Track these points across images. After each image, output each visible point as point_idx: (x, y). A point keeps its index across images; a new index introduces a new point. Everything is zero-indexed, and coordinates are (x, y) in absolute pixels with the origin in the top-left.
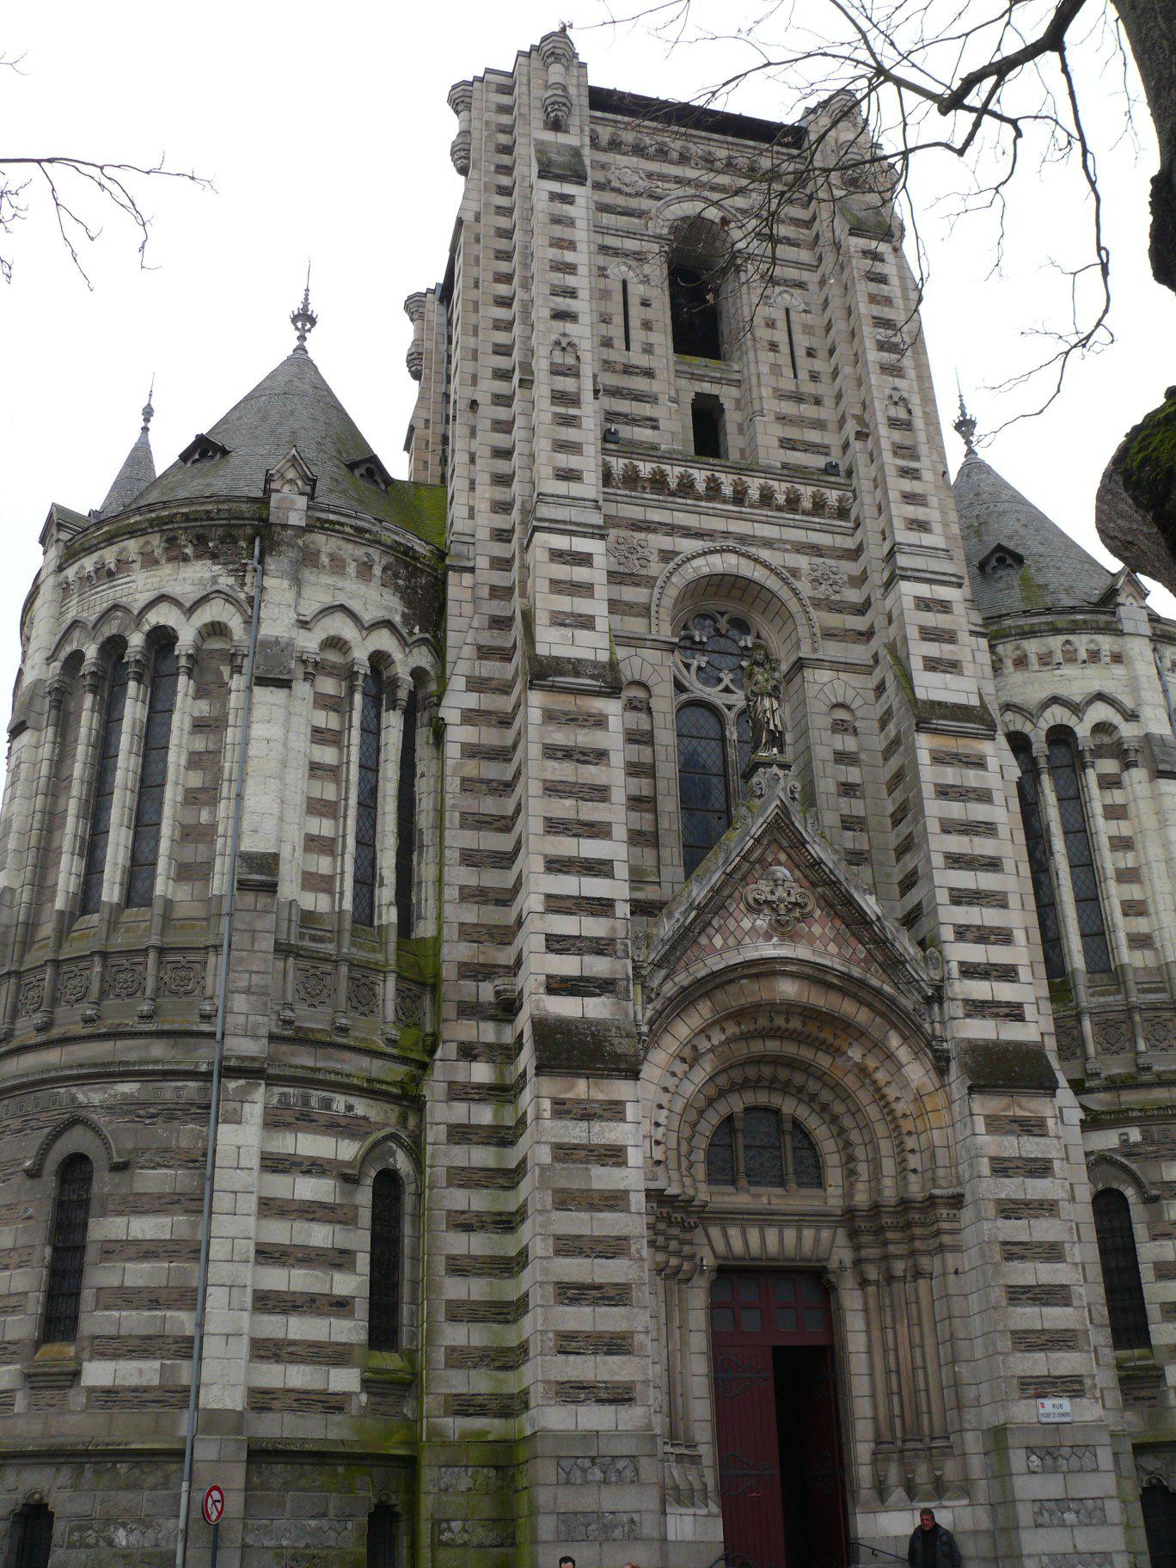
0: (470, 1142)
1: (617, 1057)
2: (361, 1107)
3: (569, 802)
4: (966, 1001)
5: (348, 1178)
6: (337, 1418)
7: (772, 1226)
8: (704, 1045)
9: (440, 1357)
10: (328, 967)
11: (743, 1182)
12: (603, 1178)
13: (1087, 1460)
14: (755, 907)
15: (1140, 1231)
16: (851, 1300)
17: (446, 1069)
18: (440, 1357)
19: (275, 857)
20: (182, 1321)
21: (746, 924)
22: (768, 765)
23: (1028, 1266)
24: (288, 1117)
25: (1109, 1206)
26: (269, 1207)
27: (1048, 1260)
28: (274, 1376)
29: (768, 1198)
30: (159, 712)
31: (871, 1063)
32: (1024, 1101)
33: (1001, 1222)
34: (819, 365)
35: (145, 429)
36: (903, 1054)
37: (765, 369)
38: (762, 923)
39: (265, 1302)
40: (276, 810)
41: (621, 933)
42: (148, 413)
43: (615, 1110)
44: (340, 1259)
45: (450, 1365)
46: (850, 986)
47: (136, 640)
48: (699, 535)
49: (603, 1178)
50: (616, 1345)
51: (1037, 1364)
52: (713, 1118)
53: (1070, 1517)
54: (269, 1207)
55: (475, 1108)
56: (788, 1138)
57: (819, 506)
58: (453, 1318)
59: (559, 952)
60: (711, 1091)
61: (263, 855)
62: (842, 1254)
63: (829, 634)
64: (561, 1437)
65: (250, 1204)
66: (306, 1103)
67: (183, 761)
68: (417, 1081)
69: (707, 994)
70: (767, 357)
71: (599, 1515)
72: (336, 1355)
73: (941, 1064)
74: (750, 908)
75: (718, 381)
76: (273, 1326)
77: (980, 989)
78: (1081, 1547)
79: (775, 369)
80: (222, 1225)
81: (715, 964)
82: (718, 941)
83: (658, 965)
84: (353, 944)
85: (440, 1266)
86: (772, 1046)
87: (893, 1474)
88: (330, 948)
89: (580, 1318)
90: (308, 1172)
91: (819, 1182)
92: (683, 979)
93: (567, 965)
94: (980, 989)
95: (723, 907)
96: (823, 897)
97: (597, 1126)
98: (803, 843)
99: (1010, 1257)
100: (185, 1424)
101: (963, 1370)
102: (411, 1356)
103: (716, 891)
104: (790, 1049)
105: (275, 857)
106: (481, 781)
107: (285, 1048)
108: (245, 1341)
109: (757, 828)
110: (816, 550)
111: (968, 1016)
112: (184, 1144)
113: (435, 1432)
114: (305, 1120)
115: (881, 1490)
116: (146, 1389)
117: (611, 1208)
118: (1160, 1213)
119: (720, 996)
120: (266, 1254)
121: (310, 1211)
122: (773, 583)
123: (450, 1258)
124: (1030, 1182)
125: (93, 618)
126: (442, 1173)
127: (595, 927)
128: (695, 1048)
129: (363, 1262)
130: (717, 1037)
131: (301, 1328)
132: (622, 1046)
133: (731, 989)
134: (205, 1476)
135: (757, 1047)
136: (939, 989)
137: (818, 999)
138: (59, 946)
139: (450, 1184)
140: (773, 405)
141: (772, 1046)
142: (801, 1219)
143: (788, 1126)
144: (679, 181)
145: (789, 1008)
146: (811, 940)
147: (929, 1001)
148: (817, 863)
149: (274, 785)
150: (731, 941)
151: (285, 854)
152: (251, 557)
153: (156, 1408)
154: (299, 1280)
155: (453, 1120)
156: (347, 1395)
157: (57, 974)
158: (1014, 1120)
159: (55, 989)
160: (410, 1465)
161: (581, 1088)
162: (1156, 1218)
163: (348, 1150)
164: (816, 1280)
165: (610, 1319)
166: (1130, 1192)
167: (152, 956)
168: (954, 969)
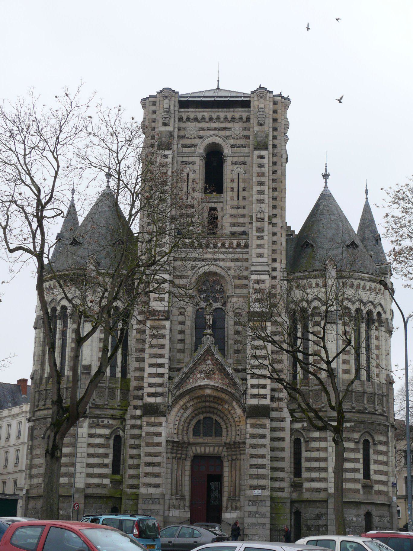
0: (135, 429)
1: (161, 412)
2: (111, 422)
3: (155, 349)
4: (251, 394)
5: (108, 438)
6: (104, 489)
7: (206, 446)
8: (188, 405)
9: (127, 476)
10: (104, 390)
11: (201, 436)
12: (156, 439)
13: (264, 504)
14: (201, 372)
15: (303, 449)
16: (226, 464)
17: (131, 411)
18: (127, 476)
19: (90, 366)
20: (72, 469)
21: (199, 376)
22: (206, 335)
23: (256, 459)
24: (94, 425)
25: (297, 444)
26: (90, 445)
27: (261, 458)
28: (91, 481)
29: (208, 440)
30: (65, 325)
31: (230, 408)
32: (261, 420)
33: (251, 449)
34: (246, 194)
35: (367, 198)
36: (236, 407)
37: (228, 199)
38: (203, 375)
39: (89, 465)
40: (90, 354)
41: (166, 382)
42: (367, 192)
43: (160, 424)
44: (106, 456)
45: (129, 478)
46: (223, 391)
47: (58, 308)
48: (203, 260)
49: (156, 439)
50: (157, 475)
51: (255, 482)
52: (195, 420)
53: (257, 516)
54: (90, 445)
55: (136, 421)
56: (214, 425)
57: (239, 245)
58: (130, 468)
59: (151, 387)
60: (193, 414)
61: (87, 365)
62: (225, 453)
63: (237, 287)
64: (144, 494)
65: (85, 445)
66: (98, 422)
67: (70, 341)
68: (124, 414)
69: (188, 394)
70: (230, 193)
71: (151, 510)
72: (105, 476)
73: (244, 410)
74: (200, 372)
75: (217, 202)
76: (90, 470)
77: (255, 391)
78: (259, 522)
79: (232, 198)
80: (79, 450)
81: (189, 387)
82: (191, 381)
83: (175, 388)
84: (110, 383)
85: (128, 456)
86: (207, 404)
87: (229, 505)
88: (104, 385)
89: (149, 470)
90: (98, 437)
91: (221, 436)
92: (181, 391)
93: (152, 390)
94: (255, 391)
95: (193, 372)
96: (219, 368)
97: (156, 428)
98: (214, 354)
99: (252, 457)
100: (73, 491)
101: (242, 482)
102: (122, 476)
103: (190, 369)
104: (212, 405)
105: (90, 366)
106: (141, 339)
107: (93, 410)
108: (84, 474)
109: (202, 352)
110: (237, 260)
111: (251, 398)
112: (72, 432)
113: (125, 492)
114: (98, 426)
115: (227, 508)
116: (65, 484)
117: (158, 446)
118: (308, 445)
119: (191, 394)
120: (89, 455)
121: (99, 446)
122: (222, 273)
123: (130, 455)
124: (259, 439)
125: (50, 300)
126: (128, 436)
127: (159, 380)
128: (186, 406)
129: (111, 456)
130: (192, 403)
131: (97, 471)
132: (162, 409)
133: (194, 392)
134: (76, 500)
135: (203, 404)
136: (245, 391)
137: (216, 394)
138: (46, 386)
139: (130, 438)
140: (230, 211)
141: (207, 404)
142: (215, 445)
143: (214, 422)
144: (209, 129)
145: (209, 396)
146: (215, 379)
147: (243, 394)
148: (217, 360)
149: (89, 347)
150: (194, 381)
151: (93, 364)
152: (83, 285)
153: (67, 487)
154: (96, 460)
155: (132, 424)
156: (107, 484)
157: (46, 393)
158: (258, 425)
159: (46, 396)
160: (120, 498)
161: (153, 419)
162: (307, 446)
163: (108, 432)
164: (217, 459)
165: (156, 470)
166: (302, 439)
167: (65, 389)
168: (249, 386)
